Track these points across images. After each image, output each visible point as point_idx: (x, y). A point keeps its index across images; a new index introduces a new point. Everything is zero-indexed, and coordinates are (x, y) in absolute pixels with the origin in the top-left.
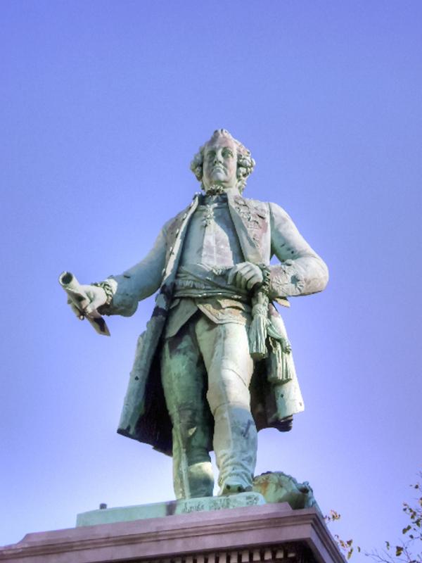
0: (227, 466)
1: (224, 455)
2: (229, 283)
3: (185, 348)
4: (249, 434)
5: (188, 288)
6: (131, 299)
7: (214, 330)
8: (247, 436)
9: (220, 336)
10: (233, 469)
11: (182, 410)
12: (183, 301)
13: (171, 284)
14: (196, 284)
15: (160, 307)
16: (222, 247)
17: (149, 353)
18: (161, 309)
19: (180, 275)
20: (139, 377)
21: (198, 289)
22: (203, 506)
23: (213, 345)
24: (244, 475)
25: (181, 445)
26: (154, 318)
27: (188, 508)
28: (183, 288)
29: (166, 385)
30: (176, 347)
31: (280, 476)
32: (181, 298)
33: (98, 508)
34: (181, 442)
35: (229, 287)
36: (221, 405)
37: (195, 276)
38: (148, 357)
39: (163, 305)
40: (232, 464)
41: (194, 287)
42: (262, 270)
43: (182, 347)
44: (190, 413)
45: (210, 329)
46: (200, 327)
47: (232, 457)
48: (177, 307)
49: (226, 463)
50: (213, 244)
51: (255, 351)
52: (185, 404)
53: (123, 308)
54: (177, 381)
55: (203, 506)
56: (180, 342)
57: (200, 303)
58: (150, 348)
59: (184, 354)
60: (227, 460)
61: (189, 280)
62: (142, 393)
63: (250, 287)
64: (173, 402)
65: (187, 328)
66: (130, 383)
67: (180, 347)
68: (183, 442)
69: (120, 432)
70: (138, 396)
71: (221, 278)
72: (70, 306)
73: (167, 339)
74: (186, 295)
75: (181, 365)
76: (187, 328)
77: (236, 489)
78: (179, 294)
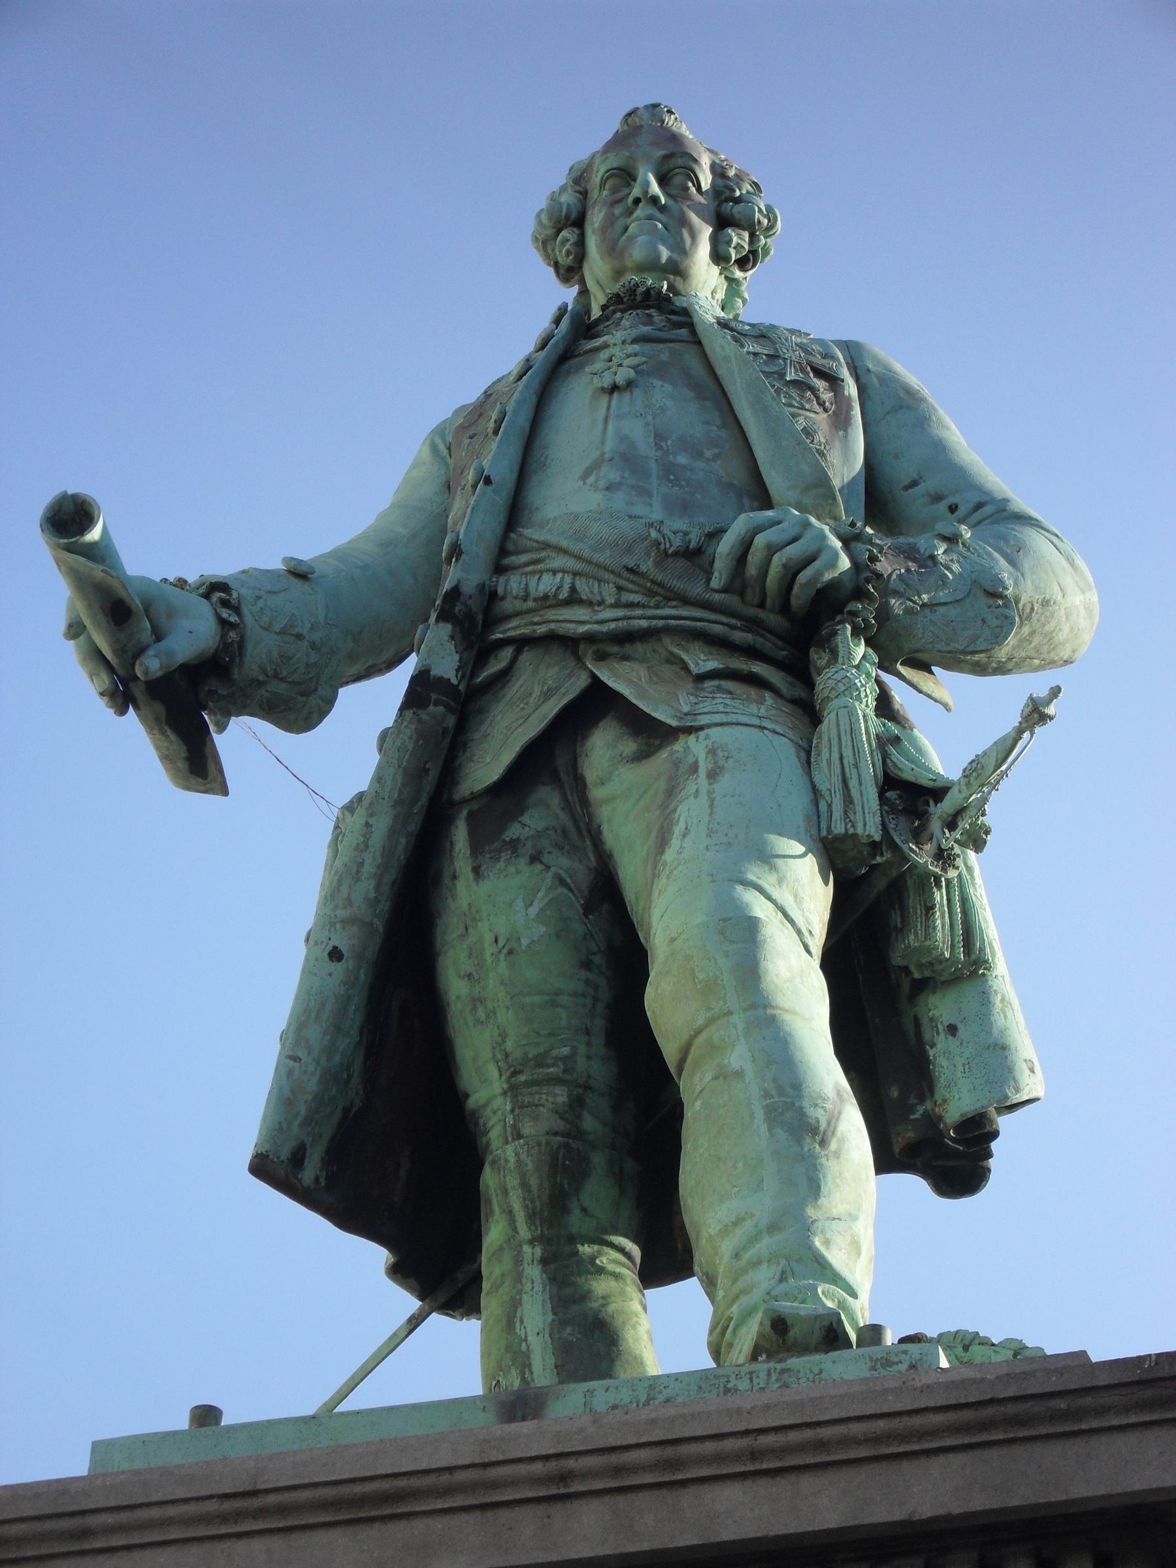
0: (755, 1264)
1: (738, 1222)
2: (715, 583)
3: (539, 834)
5: (547, 601)
6: (314, 657)
7: (664, 754)
9: (694, 768)
10: (783, 1279)
11: (528, 1084)
12: (526, 657)
13: (482, 587)
14: (582, 586)
15: (436, 672)
16: (682, 459)
17: (388, 852)
18: (442, 682)
19: (508, 561)
20: (344, 949)
21: (590, 604)
23: (663, 806)
25: (524, 1232)
26: (409, 714)
28: (531, 604)
29: (455, 987)
30: (504, 829)
32: (523, 643)
33: (182, 1422)
34: (520, 1216)
35: (717, 597)
36: (712, 1021)
37: (578, 557)
38: (383, 868)
39: (447, 666)
40: (772, 1259)
41: (573, 600)
43: (526, 833)
44: (561, 1096)
45: (642, 756)
46: (603, 749)
47: (773, 1228)
48: (505, 675)
49: (747, 1256)
51: (839, 828)
52: (540, 1061)
53: (282, 688)
54: (503, 968)
56: (515, 812)
57: (601, 657)
58: (392, 833)
59: (534, 859)
60: (754, 1239)
61: (554, 572)
62: (354, 1020)
63: (799, 597)
65: (549, 758)
66: (307, 972)
67: (514, 831)
68: (531, 1217)
69: (262, 1168)
70: (337, 1029)
71: (681, 563)
72: (70, 651)
73: (465, 801)
74: (541, 630)
75: (519, 905)
76: (549, 758)
77: (817, 1335)
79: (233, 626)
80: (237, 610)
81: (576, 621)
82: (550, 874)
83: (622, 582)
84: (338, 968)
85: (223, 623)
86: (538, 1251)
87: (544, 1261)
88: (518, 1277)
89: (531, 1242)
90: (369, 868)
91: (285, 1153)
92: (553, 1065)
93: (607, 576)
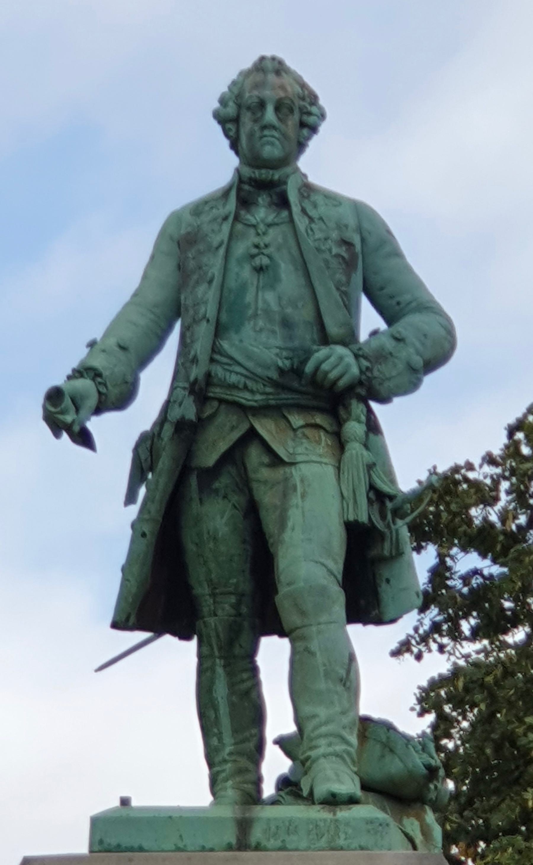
4: (351, 682)
5: (234, 387)
8: (348, 684)
14: (250, 384)
22: (296, 827)
24: (345, 756)
27: (273, 828)
31: (388, 730)
42: (357, 356)
44: (233, 599)
48: (212, 417)
50: (274, 307)
51: (351, 518)
54: (211, 545)
55: (296, 827)
59: (225, 497)
64: (202, 578)
67: (216, 485)
68: (220, 649)
69: (115, 625)
74: (229, 398)
76: (233, 456)
78: (216, 392)
79: (104, 394)
80: (105, 385)
81: (244, 398)
82: (231, 504)
83: (265, 383)
84: (144, 541)
85: (100, 393)
86: (222, 662)
87: (225, 667)
88: (213, 671)
89: (220, 658)
90: (158, 497)
91: (123, 619)
92: (230, 587)
93: (260, 380)
